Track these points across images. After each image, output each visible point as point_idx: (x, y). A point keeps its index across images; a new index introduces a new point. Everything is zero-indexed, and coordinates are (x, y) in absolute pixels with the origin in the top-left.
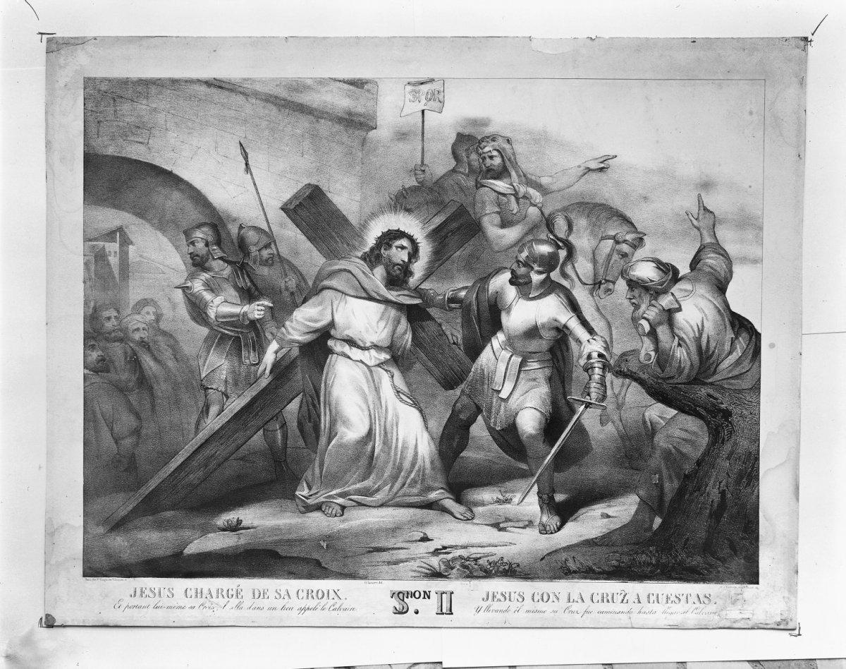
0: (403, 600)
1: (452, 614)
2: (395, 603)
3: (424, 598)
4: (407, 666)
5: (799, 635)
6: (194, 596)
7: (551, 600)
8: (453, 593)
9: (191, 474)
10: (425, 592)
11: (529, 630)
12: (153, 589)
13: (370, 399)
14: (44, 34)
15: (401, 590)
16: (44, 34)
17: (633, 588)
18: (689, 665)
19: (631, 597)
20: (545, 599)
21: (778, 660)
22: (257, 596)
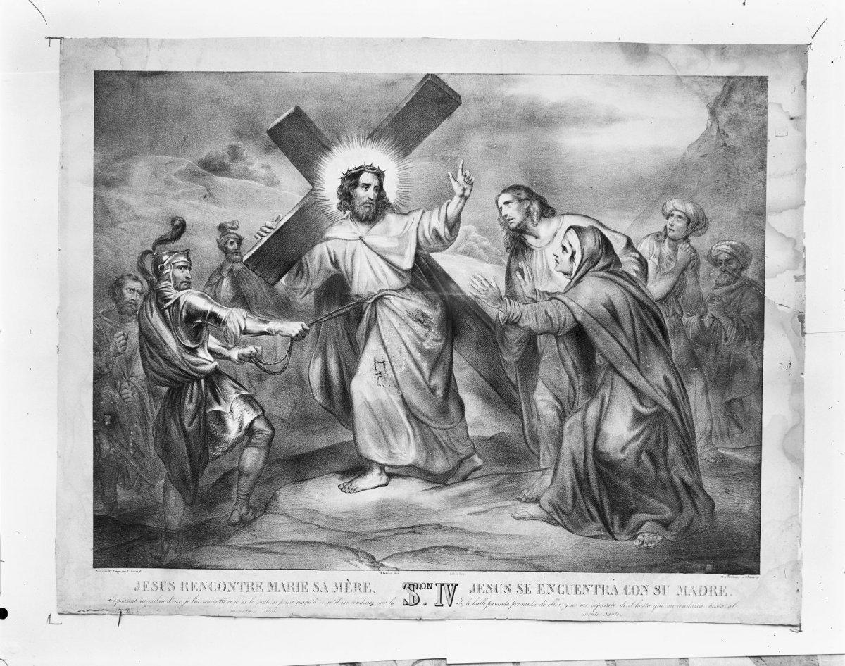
1: (442, 605)
2: (407, 595)
4: (411, 663)
5: (800, 631)
7: (227, 590)
8: (457, 585)
9: (166, 486)
10: (428, 584)
12: (508, 586)
13: (262, 365)
14: (52, 38)
15: (413, 582)
16: (52, 38)
17: (621, 579)
18: (691, 661)
20: (222, 588)
21: (773, 656)
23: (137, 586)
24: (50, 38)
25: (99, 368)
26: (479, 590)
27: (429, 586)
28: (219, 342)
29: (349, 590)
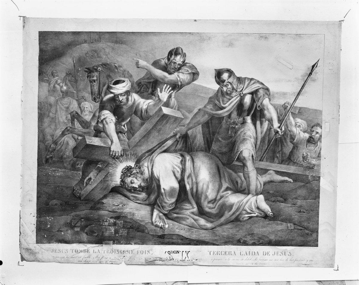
0: (170, 254)
3: (177, 253)
5: (338, 270)
6: (224, 254)
8: (190, 251)
9: (71, 202)
11: (216, 267)
12: (282, 252)
18: (291, 283)
19: (238, 253)
21: (326, 281)
22: (264, 254)
23: (274, 254)
24: (20, 16)
25: (47, 149)
26: (55, 252)
27: (178, 252)
28: (253, 152)
29: (226, 254)
